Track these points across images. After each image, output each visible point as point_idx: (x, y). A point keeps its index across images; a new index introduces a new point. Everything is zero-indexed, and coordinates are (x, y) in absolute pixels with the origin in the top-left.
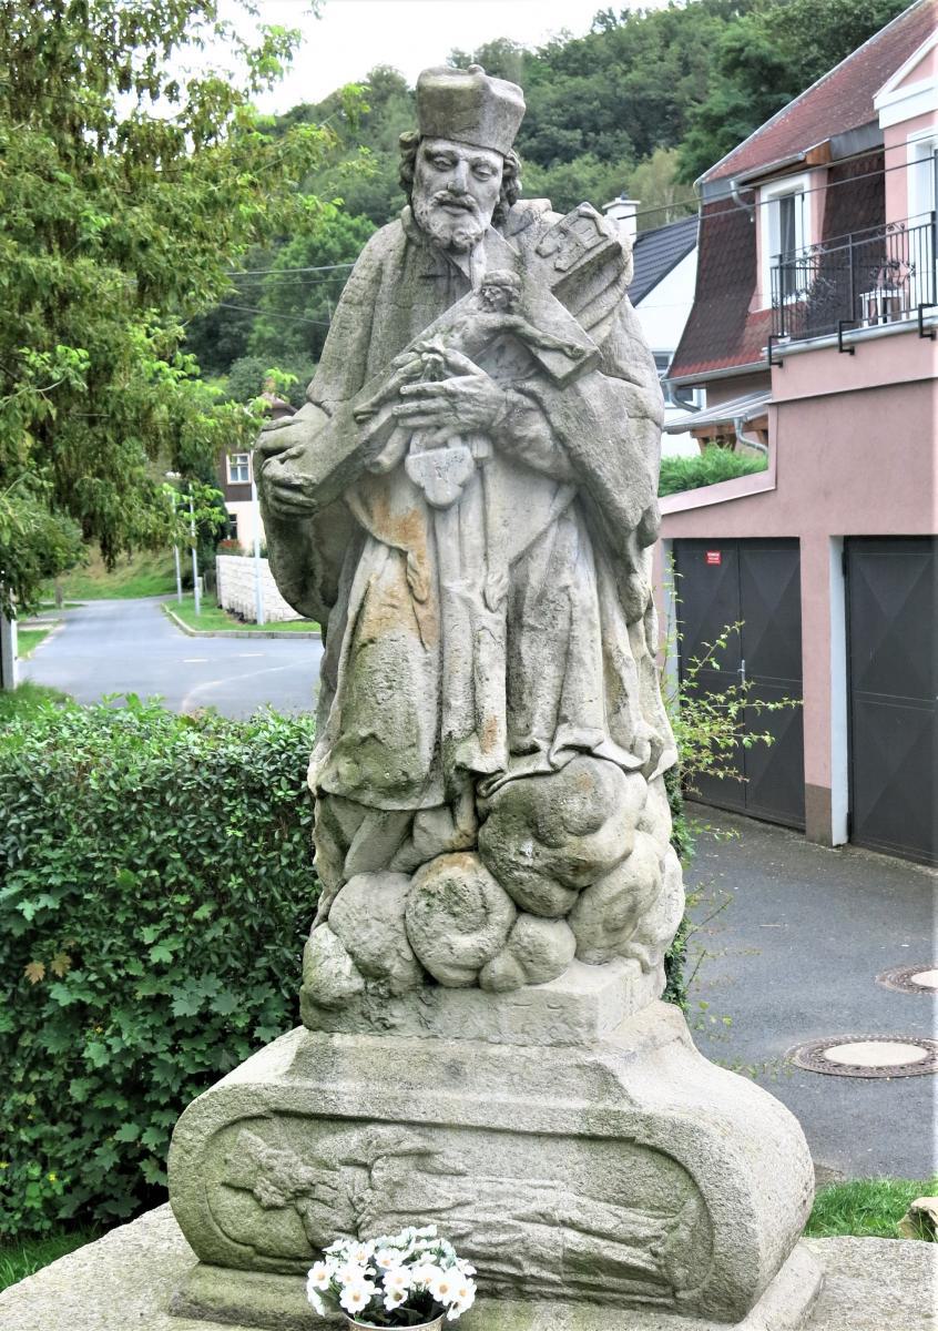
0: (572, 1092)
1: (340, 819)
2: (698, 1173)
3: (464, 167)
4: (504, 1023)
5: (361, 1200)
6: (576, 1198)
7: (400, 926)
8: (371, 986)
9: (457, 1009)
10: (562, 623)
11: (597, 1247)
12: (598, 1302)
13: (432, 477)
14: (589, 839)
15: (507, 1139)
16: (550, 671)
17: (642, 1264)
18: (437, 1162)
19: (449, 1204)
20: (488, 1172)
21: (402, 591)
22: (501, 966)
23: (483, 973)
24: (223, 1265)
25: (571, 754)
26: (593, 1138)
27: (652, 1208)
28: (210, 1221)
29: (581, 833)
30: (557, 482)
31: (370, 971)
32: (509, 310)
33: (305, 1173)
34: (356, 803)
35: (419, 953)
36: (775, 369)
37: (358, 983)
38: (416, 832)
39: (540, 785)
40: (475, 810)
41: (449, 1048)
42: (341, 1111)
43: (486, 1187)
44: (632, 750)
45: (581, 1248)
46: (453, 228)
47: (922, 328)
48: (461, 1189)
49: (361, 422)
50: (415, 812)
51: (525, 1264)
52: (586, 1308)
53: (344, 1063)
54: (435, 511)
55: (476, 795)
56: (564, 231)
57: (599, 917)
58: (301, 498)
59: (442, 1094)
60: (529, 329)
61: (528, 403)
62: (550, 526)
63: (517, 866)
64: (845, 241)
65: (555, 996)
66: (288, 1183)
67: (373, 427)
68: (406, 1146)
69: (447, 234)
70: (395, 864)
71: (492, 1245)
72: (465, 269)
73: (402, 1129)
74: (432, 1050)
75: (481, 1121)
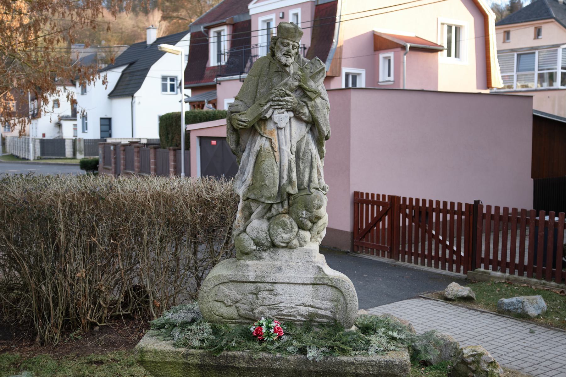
1: (252, 205)
2: (343, 291)
4: (293, 257)
5: (254, 303)
7: (268, 233)
8: (258, 248)
9: (283, 254)
11: (317, 311)
13: (280, 121)
14: (319, 210)
19: (279, 302)
20: (288, 294)
21: (270, 149)
22: (295, 242)
23: (290, 244)
25: (315, 190)
27: (331, 301)
29: (317, 209)
30: (307, 123)
33: (239, 297)
34: (259, 201)
35: (273, 239)
36: (218, 85)
38: (272, 209)
39: (308, 197)
41: (278, 263)
43: (288, 298)
45: (313, 312)
46: (286, 61)
53: (250, 268)
55: (289, 199)
56: (312, 63)
57: (317, 230)
58: (245, 124)
59: (276, 275)
60: (305, 86)
61: (304, 104)
63: (301, 217)
64: (242, 48)
65: (307, 250)
66: (234, 299)
67: (265, 108)
68: (267, 288)
69: (285, 62)
70: (265, 217)
71: (289, 312)
72: (288, 70)
75: (287, 281)
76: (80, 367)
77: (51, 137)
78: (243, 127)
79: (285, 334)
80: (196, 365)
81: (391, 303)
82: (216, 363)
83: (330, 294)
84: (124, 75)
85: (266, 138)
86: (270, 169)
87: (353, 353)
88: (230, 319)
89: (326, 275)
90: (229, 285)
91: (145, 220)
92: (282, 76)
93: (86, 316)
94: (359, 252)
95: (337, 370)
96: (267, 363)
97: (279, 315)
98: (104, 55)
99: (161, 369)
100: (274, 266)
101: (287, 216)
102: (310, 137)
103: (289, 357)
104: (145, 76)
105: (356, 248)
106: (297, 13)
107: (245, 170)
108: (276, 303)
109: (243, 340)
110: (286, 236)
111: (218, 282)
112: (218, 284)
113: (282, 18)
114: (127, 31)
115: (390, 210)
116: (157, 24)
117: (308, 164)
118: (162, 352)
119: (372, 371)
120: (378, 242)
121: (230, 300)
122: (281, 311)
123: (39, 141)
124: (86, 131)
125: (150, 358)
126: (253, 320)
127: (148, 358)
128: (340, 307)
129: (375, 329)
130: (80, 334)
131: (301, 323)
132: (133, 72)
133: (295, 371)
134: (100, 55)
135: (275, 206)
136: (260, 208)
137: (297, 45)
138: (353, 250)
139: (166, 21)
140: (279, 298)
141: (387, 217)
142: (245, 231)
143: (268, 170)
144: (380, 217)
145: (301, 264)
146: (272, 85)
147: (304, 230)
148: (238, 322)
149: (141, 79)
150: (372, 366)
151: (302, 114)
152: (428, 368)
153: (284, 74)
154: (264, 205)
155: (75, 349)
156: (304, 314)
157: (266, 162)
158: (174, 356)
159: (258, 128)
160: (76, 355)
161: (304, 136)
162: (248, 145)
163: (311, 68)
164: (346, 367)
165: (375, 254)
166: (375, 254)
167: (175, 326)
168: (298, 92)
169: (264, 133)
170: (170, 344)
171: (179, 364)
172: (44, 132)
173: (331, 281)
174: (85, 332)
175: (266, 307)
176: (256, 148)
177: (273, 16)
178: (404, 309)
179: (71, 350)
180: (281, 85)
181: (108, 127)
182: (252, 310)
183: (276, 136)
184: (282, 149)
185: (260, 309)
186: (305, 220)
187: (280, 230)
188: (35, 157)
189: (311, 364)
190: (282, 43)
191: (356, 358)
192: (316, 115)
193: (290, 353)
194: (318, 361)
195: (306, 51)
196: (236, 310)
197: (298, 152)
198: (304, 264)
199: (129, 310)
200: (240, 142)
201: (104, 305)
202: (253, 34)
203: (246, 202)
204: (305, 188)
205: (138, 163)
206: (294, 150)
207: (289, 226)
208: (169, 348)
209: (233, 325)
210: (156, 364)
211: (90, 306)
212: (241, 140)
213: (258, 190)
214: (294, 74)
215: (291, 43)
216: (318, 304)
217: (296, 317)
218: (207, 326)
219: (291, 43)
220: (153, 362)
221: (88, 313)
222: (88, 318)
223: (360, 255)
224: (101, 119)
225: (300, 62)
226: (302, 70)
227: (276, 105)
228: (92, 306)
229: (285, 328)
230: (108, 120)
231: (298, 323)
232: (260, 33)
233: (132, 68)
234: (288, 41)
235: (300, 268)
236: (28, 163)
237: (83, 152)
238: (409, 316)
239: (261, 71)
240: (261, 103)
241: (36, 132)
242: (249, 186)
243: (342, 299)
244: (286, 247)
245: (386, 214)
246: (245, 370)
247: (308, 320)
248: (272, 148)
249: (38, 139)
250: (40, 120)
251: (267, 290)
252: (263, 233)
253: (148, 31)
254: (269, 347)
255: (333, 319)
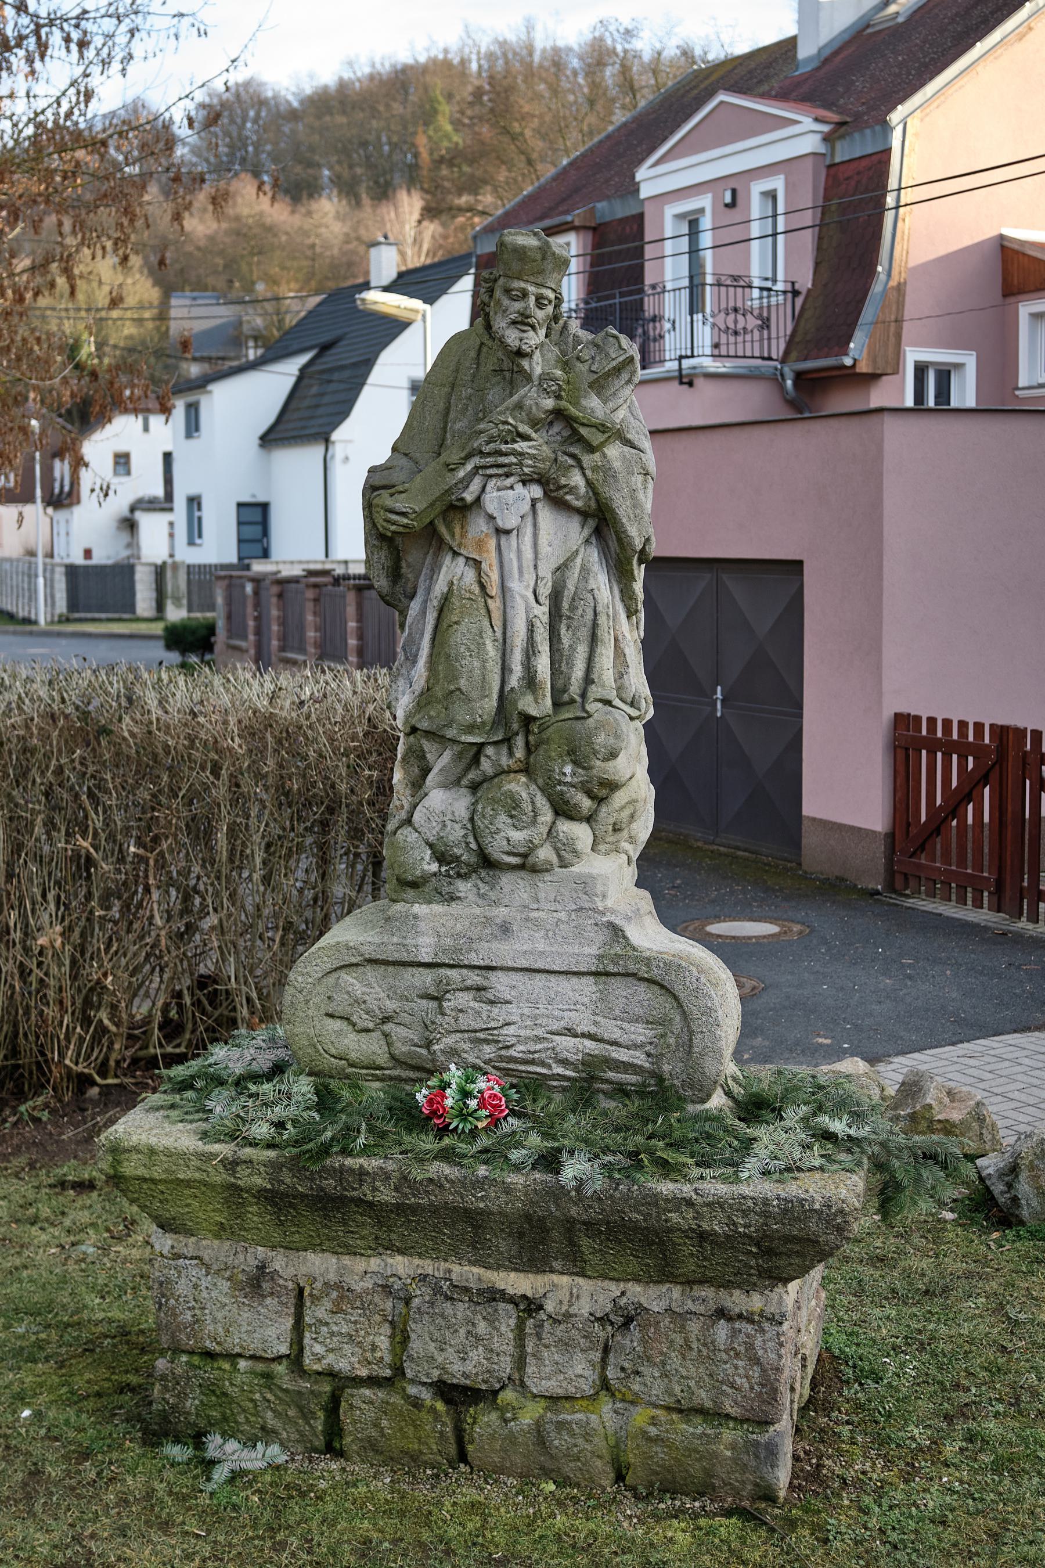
0: (590, 942)
2: (681, 996)
4: (542, 895)
5: (433, 1023)
7: (469, 826)
11: (608, 1051)
13: (502, 510)
14: (611, 763)
15: (543, 976)
19: (500, 1024)
20: (527, 1001)
21: (476, 589)
22: (545, 853)
25: (600, 705)
27: (648, 1022)
29: (606, 760)
30: (584, 514)
33: (391, 1005)
34: (443, 737)
38: (483, 759)
39: (578, 725)
40: (527, 743)
41: (501, 913)
43: (526, 1011)
47: (681, 376)
53: (422, 926)
54: (501, 532)
55: (528, 732)
56: (597, 346)
57: (611, 820)
58: (406, 521)
59: (495, 945)
60: (573, 411)
61: (570, 462)
63: (560, 783)
65: (580, 875)
67: (461, 474)
68: (469, 983)
69: (517, 343)
70: (465, 782)
71: (530, 1052)
72: (527, 367)
74: (488, 914)
75: (524, 963)
76: (31, 1195)
77: (109, 558)
78: (401, 529)
79: (513, 1113)
80: (259, 1192)
81: (962, 1042)
82: (312, 1189)
83: (646, 1003)
84: (306, 381)
85: (467, 558)
86: (472, 647)
87: (696, 1172)
88: (367, 1068)
89: (634, 949)
90: (364, 973)
91: (220, 791)
92: (511, 382)
93: (62, 1055)
94: (908, 892)
95: (645, 1220)
96: (451, 1193)
97: (502, 1059)
98: (259, 321)
99: (167, 1200)
100: (488, 921)
101: (524, 779)
102: (593, 555)
103: (512, 1178)
104: (362, 384)
105: (899, 883)
106: (775, 190)
107: (418, 650)
108: (493, 1024)
109: (395, 1126)
110: (517, 836)
111: (329, 965)
112: (335, 970)
113: (732, 205)
114: (328, 253)
115: (997, 767)
116: (409, 230)
117: (584, 633)
118: (169, 1153)
119: (745, 1226)
120: (962, 862)
121: (367, 1013)
122: (508, 1047)
123: (63, 569)
124: (198, 541)
125: (136, 1168)
126: (427, 1070)
127: (131, 1167)
128: (672, 1041)
129: (780, 1109)
130: (46, 1105)
131: (566, 1084)
132: (330, 371)
133: (528, 1217)
134: (249, 322)
135: (490, 751)
136: (447, 756)
137: (551, 295)
138: (891, 886)
139: (436, 222)
140: (503, 1012)
141: (987, 790)
142: (409, 821)
143: (469, 650)
144: (968, 793)
145: (563, 915)
146: (484, 410)
147: (571, 818)
148: (391, 1078)
149: (350, 389)
150: (745, 1213)
151: (566, 490)
152: (1010, 1234)
153: (518, 378)
154: (457, 748)
155: (28, 1148)
157: (463, 628)
158: (199, 1163)
159: (443, 530)
160: (29, 1164)
161: (577, 551)
162: (422, 578)
163: (593, 358)
164: (670, 1211)
165: (954, 897)
166: (954, 897)
167: (221, 1082)
168: (556, 428)
169: (460, 545)
170: (195, 1133)
171: (212, 1186)
172: (87, 546)
173: (648, 965)
174: (60, 1101)
175: (466, 1035)
176: (440, 587)
177: (705, 201)
178: (995, 1059)
179: (17, 1151)
180: (507, 409)
181: (259, 529)
182: (428, 1045)
183: (494, 554)
184: (509, 589)
185: (449, 1041)
186: (572, 790)
187: (503, 818)
188: (53, 615)
189: (571, 1198)
190: (507, 291)
191: (700, 1186)
192: (606, 492)
193: (517, 1168)
194: (589, 1194)
195: (799, 301)
196: (383, 1042)
197: (556, 597)
198: (573, 917)
199: (184, 1044)
200: (403, 571)
201: (113, 1029)
202: (649, 251)
203: (412, 738)
204: (573, 701)
205: (316, 631)
206: (545, 591)
207: (527, 807)
208: (187, 1143)
209: (377, 1085)
210: (153, 1187)
211: (75, 1028)
212: (404, 564)
213: (439, 706)
214: (545, 377)
215: (531, 289)
216: (611, 1030)
217: (550, 1067)
218: (303, 1087)
219: (531, 289)
220: (145, 1180)
221: (68, 1048)
222: (67, 1062)
223: (911, 902)
224: (240, 505)
225: (566, 344)
226: (566, 365)
227: (491, 466)
228: (78, 1030)
229: (516, 1096)
230: (259, 510)
231: (555, 1083)
232: (669, 247)
233: (331, 359)
234: (523, 285)
235: (562, 926)
236: (31, 633)
237: (185, 602)
238: (1002, 1080)
239: (457, 371)
240: (450, 461)
241: (68, 543)
242: (422, 694)
243: (678, 1018)
244: (521, 867)
245: (985, 780)
246: (391, 1211)
247: (584, 1075)
248: (482, 587)
249: (61, 565)
250: (77, 510)
251: (468, 989)
252: (457, 826)
253: (373, 251)
254: (463, 1147)
255: (653, 1074)
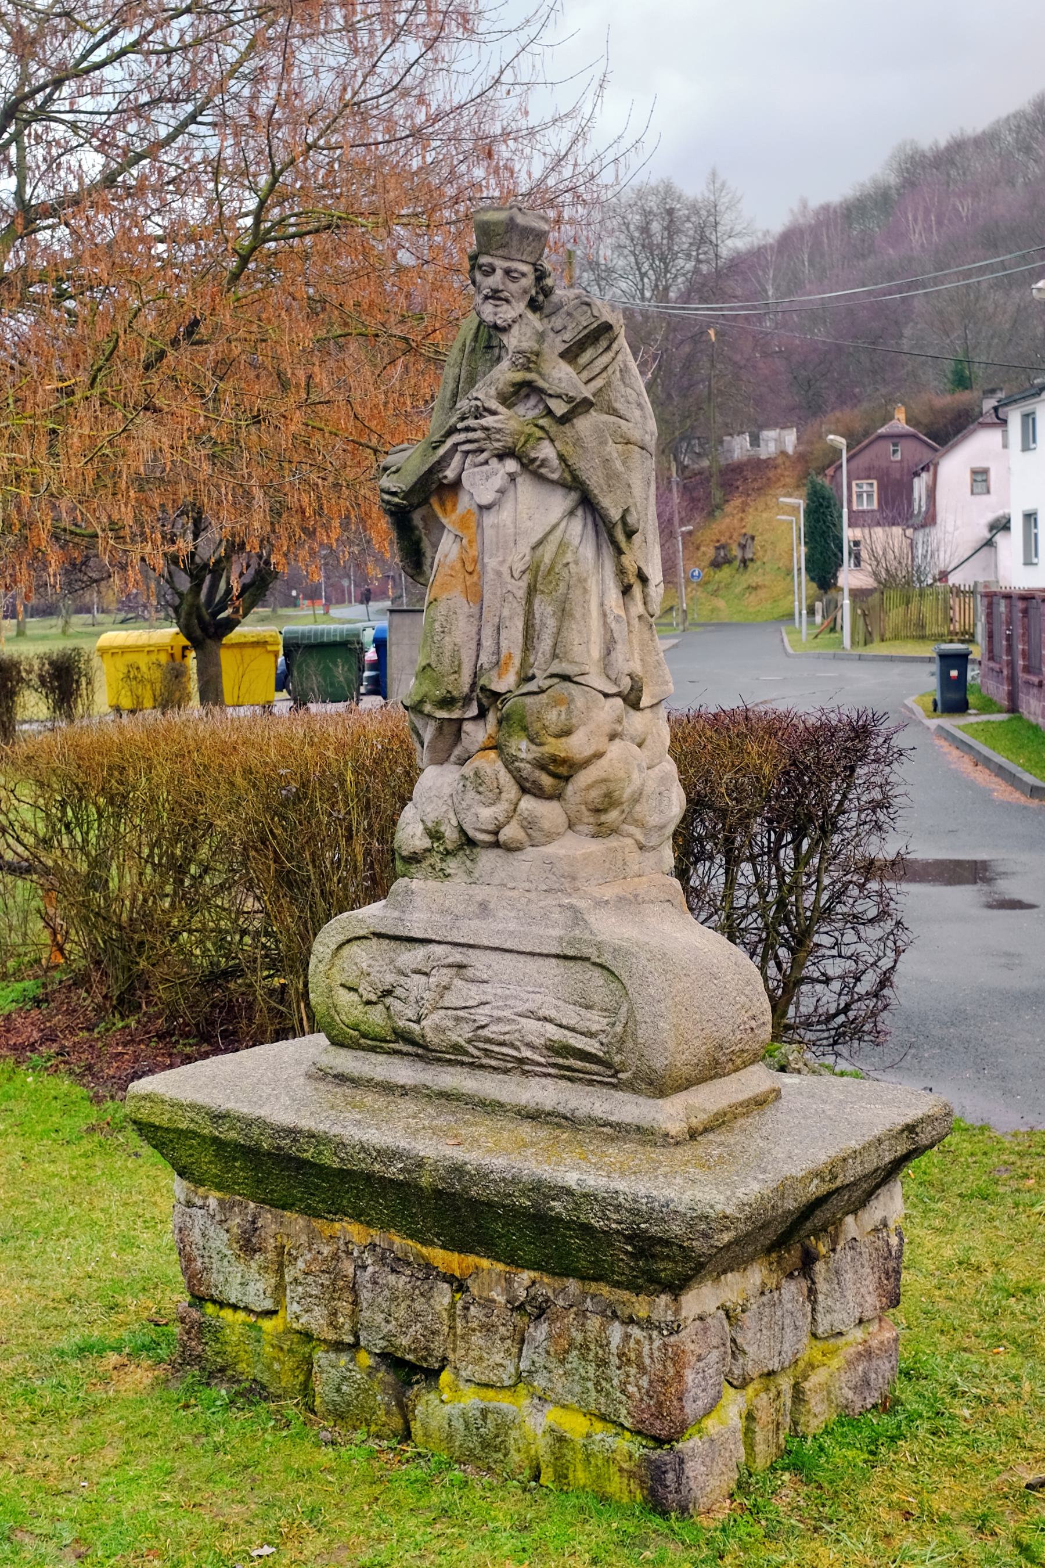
3: (499, 272)
6: (554, 1001)
7: (450, 802)
9: (487, 859)
10: (562, 587)
11: (565, 1036)
12: (570, 1079)
16: (551, 623)
17: (594, 1051)
18: (469, 973)
24: (342, 1045)
25: (556, 680)
26: (566, 957)
27: (601, 1010)
28: (333, 1012)
30: (561, 484)
31: (435, 835)
32: (528, 369)
33: (390, 978)
37: (427, 843)
38: (463, 735)
39: (529, 700)
42: (413, 934)
43: (499, 991)
44: (616, 682)
48: (484, 992)
49: (435, 448)
50: (460, 721)
51: (523, 1048)
52: (564, 1084)
53: (418, 901)
59: (475, 923)
60: (541, 383)
62: (562, 520)
67: (441, 451)
70: (452, 758)
73: (449, 947)
122: (482, 1027)
150: (618, 1208)
156: (539, 1042)
175: (450, 1012)
251: (450, 966)
